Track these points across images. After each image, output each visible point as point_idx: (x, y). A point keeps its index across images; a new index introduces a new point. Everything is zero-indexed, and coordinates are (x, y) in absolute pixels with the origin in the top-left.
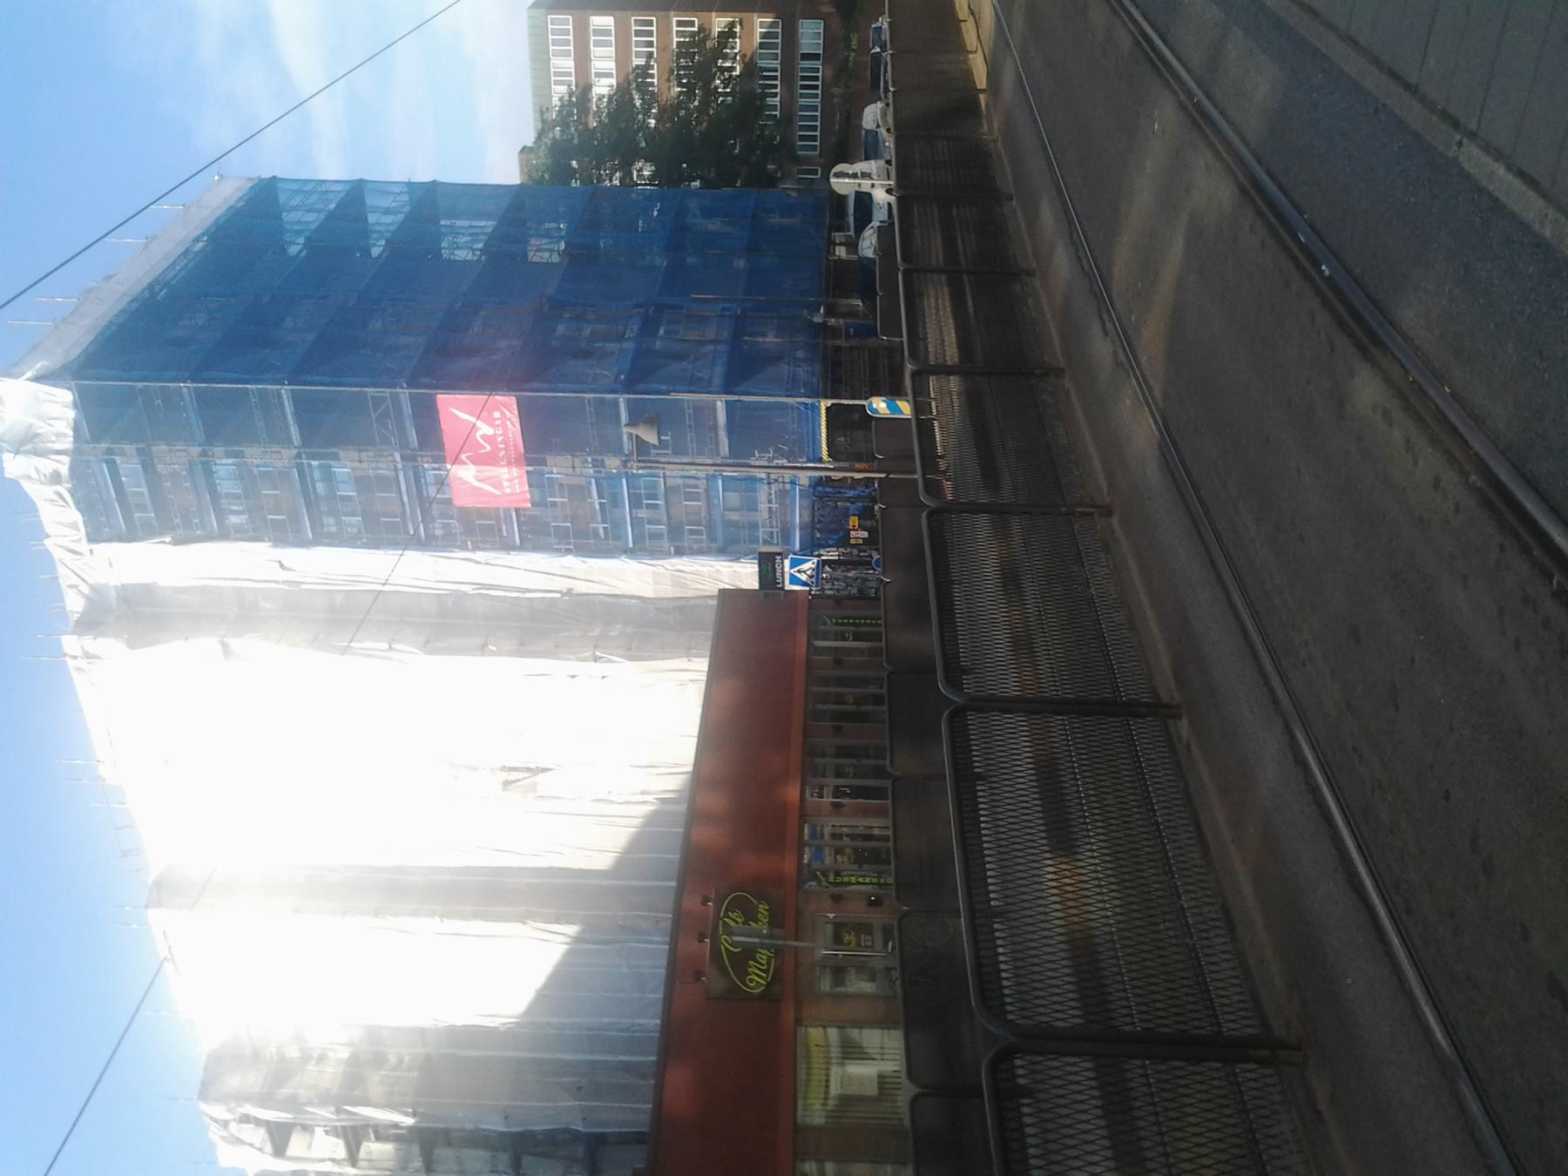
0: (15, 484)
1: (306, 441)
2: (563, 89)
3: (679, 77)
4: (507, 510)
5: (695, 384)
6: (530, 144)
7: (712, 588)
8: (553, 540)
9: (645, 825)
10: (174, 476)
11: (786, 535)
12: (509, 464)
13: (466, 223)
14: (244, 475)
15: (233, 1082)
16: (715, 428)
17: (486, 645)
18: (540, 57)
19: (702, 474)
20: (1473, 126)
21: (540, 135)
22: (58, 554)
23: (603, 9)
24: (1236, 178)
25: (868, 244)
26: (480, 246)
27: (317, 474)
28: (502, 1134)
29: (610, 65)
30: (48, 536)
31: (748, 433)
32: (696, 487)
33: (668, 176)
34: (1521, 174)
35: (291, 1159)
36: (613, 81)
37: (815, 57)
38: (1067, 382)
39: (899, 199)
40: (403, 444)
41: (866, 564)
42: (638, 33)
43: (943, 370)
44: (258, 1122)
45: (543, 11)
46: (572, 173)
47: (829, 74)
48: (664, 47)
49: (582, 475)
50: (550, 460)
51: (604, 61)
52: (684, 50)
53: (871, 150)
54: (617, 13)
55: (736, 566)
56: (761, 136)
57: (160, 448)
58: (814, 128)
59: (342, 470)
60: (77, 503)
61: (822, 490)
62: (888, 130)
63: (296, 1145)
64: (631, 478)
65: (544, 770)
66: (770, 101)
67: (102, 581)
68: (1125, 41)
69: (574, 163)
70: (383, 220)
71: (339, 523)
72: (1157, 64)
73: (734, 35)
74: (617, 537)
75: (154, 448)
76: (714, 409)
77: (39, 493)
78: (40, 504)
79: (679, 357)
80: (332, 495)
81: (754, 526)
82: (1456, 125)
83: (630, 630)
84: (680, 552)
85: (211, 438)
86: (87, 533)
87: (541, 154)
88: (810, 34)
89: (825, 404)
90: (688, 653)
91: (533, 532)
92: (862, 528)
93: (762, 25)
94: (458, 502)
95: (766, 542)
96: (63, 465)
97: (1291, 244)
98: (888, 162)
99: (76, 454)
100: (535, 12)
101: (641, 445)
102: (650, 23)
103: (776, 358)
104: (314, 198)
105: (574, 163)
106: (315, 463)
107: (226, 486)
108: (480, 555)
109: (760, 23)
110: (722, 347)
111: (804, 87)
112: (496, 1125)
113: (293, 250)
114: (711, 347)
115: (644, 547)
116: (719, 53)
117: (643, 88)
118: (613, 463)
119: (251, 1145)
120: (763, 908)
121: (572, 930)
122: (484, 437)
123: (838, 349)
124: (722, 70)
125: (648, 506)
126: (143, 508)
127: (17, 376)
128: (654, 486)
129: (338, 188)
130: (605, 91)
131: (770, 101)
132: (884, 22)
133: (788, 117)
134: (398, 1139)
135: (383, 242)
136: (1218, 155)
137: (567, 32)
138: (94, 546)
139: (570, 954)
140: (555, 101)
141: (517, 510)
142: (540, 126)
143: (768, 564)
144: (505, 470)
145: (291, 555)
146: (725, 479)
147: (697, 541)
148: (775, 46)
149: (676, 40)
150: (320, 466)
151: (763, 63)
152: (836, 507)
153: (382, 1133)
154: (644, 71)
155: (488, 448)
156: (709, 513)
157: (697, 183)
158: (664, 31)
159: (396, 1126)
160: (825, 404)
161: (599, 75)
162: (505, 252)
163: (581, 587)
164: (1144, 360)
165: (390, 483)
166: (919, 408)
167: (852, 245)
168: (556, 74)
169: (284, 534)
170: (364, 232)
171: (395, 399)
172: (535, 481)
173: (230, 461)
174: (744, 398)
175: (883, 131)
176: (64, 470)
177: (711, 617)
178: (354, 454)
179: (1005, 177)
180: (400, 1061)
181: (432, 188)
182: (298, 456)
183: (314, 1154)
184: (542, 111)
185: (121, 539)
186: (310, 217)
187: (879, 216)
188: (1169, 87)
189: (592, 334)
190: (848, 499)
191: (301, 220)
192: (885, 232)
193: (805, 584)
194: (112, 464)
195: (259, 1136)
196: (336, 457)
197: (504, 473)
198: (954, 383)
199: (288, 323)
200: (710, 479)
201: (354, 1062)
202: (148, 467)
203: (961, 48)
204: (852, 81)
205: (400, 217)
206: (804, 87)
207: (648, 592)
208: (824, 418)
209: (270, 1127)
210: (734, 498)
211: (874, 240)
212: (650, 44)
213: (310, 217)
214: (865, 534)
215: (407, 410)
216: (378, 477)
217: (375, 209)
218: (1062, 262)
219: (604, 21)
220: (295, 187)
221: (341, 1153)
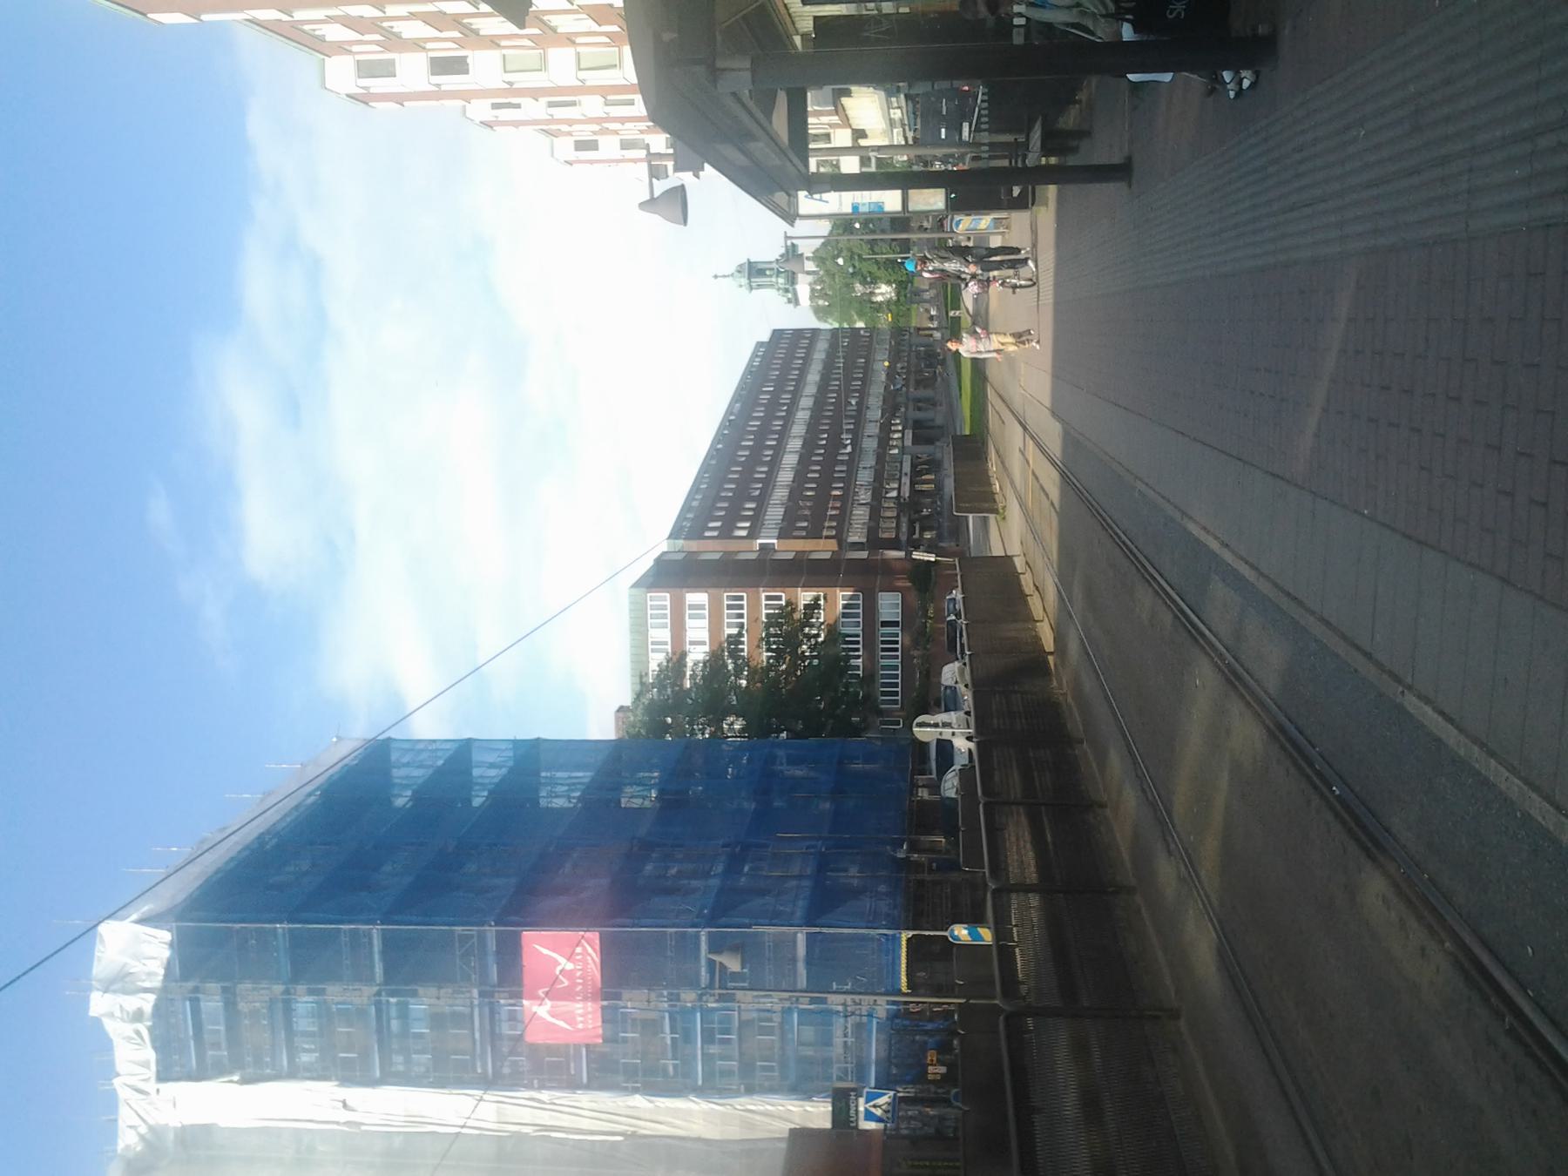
0: (97, 1021)
1: (387, 981)
3: (768, 643)
4: (577, 1047)
5: (775, 918)
8: (620, 1078)
11: (861, 1074)
12: (585, 999)
13: (565, 775)
14: (324, 1015)
16: (794, 960)
18: (639, 628)
19: (778, 1007)
20: (1409, 680)
21: (638, 696)
22: (123, 1094)
23: (697, 587)
24: (1263, 722)
25: (950, 785)
26: (577, 794)
27: (393, 1012)
29: (704, 635)
30: (118, 1075)
31: (828, 966)
32: (770, 1020)
33: (759, 728)
34: (1442, 713)
37: (895, 624)
38: (1138, 899)
39: (979, 744)
40: (484, 980)
41: (946, 1102)
42: (729, 607)
43: (1026, 889)
46: (666, 728)
47: (907, 641)
48: (754, 619)
50: (626, 994)
51: (698, 632)
52: (772, 621)
53: (952, 704)
54: (713, 591)
55: (809, 1107)
56: (847, 693)
57: (244, 987)
58: (896, 685)
59: (418, 1007)
60: (153, 1041)
61: (903, 1024)
64: (706, 1013)
66: (853, 662)
67: (162, 1122)
68: (1168, 618)
69: (669, 720)
71: (408, 1061)
72: (1195, 635)
73: (818, 606)
75: (240, 987)
76: (795, 942)
77: (117, 1029)
78: (117, 1041)
79: (762, 893)
80: (405, 1033)
81: (827, 1062)
82: (1399, 680)
84: (750, 1091)
85: (296, 978)
86: (158, 1072)
87: (639, 712)
88: (889, 605)
89: (905, 935)
91: (606, 1069)
92: (940, 1063)
95: (840, 1079)
96: (147, 1002)
97: (1308, 770)
98: (968, 713)
100: (638, 591)
101: (721, 977)
102: (741, 598)
103: (856, 893)
105: (669, 720)
107: (303, 1024)
108: (545, 1095)
109: (841, 596)
110: (806, 883)
111: (884, 650)
113: (399, 802)
114: (794, 883)
115: (711, 1087)
117: (735, 654)
118: (688, 997)
123: (921, 883)
124: (809, 637)
125: (723, 1041)
126: (216, 1046)
127: (123, 919)
128: (729, 1019)
129: (448, 746)
130: (701, 657)
131: (853, 662)
132: (957, 594)
133: (869, 677)
136: (1248, 704)
137: (664, 607)
138: (162, 1086)
141: (587, 1046)
142: (638, 688)
143: (842, 1103)
144: (579, 1005)
145: (356, 1095)
146: (802, 1012)
149: (765, 612)
150: (398, 1004)
152: (914, 1041)
154: (735, 640)
155: (566, 983)
156: (782, 1048)
157: (784, 735)
158: (753, 606)
160: (905, 935)
162: (601, 803)
163: (647, 1128)
164: (1203, 873)
166: (1001, 933)
167: (935, 787)
169: (354, 1074)
170: (467, 785)
171: (482, 938)
172: (611, 1017)
173: (311, 999)
174: (825, 930)
175: (961, 687)
178: (433, 991)
179: (1075, 723)
181: (537, 743)
182: (378, 994)
184: (642, 676)
187: (960, 761)
188: (1207, 654)
189: (679, 872)
190: (926, 1032)
191: (407, 778)
192: (966, 774)
193: (879, 1120)
194: (195, 1002)
196: (414, 994)
197: (578, 1007)
198: (1034, 900)
199: (387, 868)
200: (787, 1012)
202: (230, 1004)
203: (1030, 619)
204: (928, 642)
205: (504, 771)
206: (884, 650)
208: (904, 950)
210: (809, 1033)
211: (956, 782)
212: (741, 616)
214: (943, 1070)
215: (492, 945)
216: (454, 1014)
218: (1130, 799)
219: (698, 598)
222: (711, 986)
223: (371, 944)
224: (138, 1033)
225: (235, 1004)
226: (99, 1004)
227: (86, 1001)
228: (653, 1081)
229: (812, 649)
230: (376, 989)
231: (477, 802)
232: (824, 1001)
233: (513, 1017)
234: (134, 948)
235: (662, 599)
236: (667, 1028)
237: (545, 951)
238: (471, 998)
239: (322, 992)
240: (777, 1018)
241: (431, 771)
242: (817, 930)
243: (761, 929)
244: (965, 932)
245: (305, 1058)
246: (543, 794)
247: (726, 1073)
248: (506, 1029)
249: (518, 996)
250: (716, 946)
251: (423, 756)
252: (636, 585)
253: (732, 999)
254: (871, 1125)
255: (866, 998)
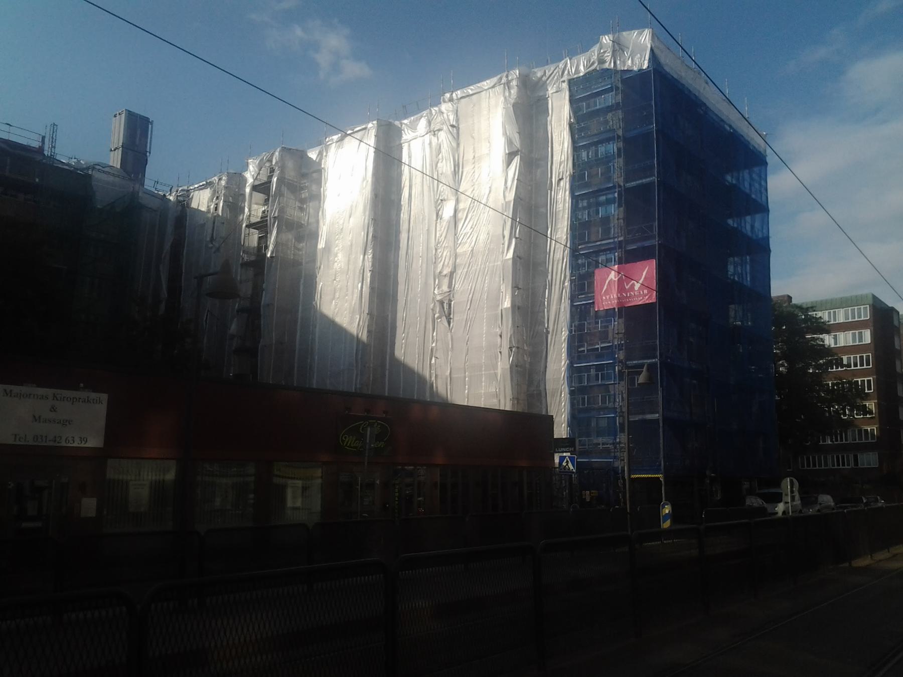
0: (597, 41)
1: (627, 190)
2: (826, 318)
3: (837, 384)
6: (794, 301)
7: (552, 412)
8: (577, 323)
9: (419, 375)
10: (607, 122)
11: (582, 454)
12: (618, 298)
15: (290, 164)
16: (644, 413)
17: (519, 289)
18: (843, 303)
21: (800, 308)
23: (874, 336)
25: (754, 502)
27: (610, 196)
28: (260, 303)
29: (841, 343)
31: (641, 433)
35: (251, 194)
36: (833, 346)
39: (780, 519)
40: (627, 242)
42: (861, 358)
44: (270, 177)
45: (871, 302)
49: (614, 338)
51: (844, 339)
54: (872, 345)
57: (620, 114)
58: (814, 465)
59: (613, 209)
61: (611, 474)
62: (819, 511)
63: (259, 197)
64: (612, 366)
65: (449, 323)
70: (748, 224)
71: (584, 208)
74: (579, 357)
80: (599, 204)
83: (527, 366)
84: (572, 393)
85: (626, 140)
87: (789, 309)
88: (870, 460)
90: (516, 399)
91: (582, 313)
92: (592, 498)
93: (872, 430)
94: (597, 271)
96: (609, 65)
98: (801, 511)
99: (615, 71)
100: (871, 296)
101: (635, 371)
102: (868, 364)
104: (757, 185)
106: (616, 195)
108: (567, 284)
112: (264, 300)
113: (729, 178)
115: (574, 372)
116: (853, 407)
117: (830, 364)
118: (621, 355)
119: (259, 174)
120: (381, 444)
121: (364, 337)
122: (633, 285)
125: (597, 375)
126: (588, 106)
129: (764, 198)
130: (827, 342)
132: (881, 503)
134: (259, 248)
135: (735, 225)
137: (860, 316)
139: (351, 335)
140: (819, 314)
142: (805, 306)
145: (566, 184)
147: (578, 402)
148: (860, 439)
151: (849, 433)
153: (263, 239)
154: (839, 363)
158: (864, 373)
159: (267, 247)
161: (835, 338)
165: (606, 233)
166: (668, 533)
168: (835, 312)
169: (577, 180)
172: (609, 313)
173: (616, 150)
174: (661, 430)
175: (818, 507)
176: (606, 66)
177: (535, 411)
178: (621, 216)
180: (299, 250)
182: (620, 186)
183: (255, 207)
184: (813, 308)
185: (571, 96)
186: (747, 184)
192: (762, 511)
194: (611, 90)
195: (264, 178)
196: (620, 206)
197: (614, 295)
201: (300, 226)
202: (610, 109)
205: (749, 234)
207: (549, 375)
209: (269, 182)
210: (603, 423)
212: (856, 365)
213: (747, 184)
216: (610, 228)
217: (753, 221)
219: (867, 337)
220: (763, 176)
221: (254, 220)
222: (628, 367)
223: (646, 177)
224: (593, 64)
225: (611, 111)
226: (606, 40)
227: (604, 34)
228: (577, 340)
229: (837, 412)
230: (622, 184)
231: (730, 222)
232: (622, 430)
233: (608, 261)
234: (638, 49)
235: (865, 314)
236: (603, 345)
237: (644, 274)
238: (618, 237)
239: (619, 156)
240: (611, 405)
241: (748, 191)
242: (661, 425)
243: (660, 393)
244: (667, 511)
245: (584, 154)
246: (736, 259)
247: (580, 380)
248: (602, 258)
249: (620, 262)
250: (651, 367)
251: (757, 185)
252: (874, 297)
253: (621, 378)
254: (557, 460)
255: (626, 454)
